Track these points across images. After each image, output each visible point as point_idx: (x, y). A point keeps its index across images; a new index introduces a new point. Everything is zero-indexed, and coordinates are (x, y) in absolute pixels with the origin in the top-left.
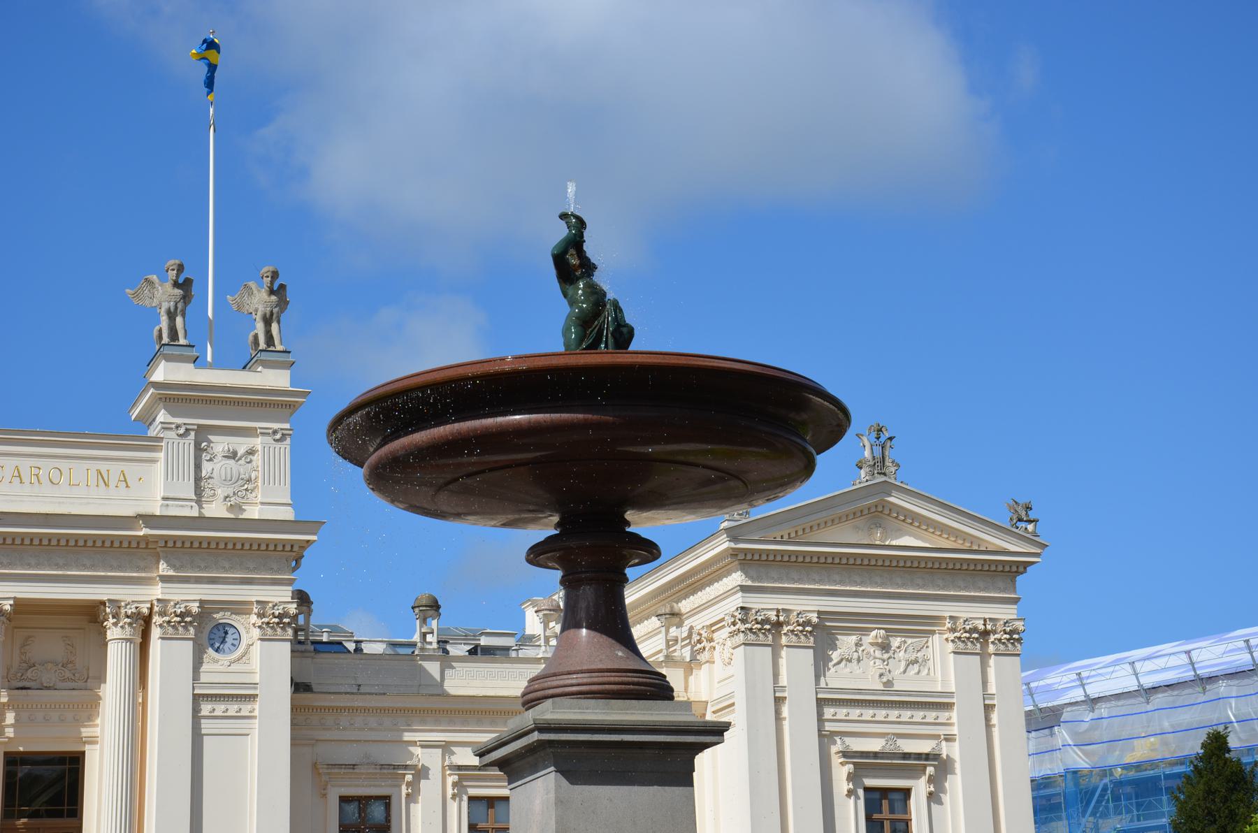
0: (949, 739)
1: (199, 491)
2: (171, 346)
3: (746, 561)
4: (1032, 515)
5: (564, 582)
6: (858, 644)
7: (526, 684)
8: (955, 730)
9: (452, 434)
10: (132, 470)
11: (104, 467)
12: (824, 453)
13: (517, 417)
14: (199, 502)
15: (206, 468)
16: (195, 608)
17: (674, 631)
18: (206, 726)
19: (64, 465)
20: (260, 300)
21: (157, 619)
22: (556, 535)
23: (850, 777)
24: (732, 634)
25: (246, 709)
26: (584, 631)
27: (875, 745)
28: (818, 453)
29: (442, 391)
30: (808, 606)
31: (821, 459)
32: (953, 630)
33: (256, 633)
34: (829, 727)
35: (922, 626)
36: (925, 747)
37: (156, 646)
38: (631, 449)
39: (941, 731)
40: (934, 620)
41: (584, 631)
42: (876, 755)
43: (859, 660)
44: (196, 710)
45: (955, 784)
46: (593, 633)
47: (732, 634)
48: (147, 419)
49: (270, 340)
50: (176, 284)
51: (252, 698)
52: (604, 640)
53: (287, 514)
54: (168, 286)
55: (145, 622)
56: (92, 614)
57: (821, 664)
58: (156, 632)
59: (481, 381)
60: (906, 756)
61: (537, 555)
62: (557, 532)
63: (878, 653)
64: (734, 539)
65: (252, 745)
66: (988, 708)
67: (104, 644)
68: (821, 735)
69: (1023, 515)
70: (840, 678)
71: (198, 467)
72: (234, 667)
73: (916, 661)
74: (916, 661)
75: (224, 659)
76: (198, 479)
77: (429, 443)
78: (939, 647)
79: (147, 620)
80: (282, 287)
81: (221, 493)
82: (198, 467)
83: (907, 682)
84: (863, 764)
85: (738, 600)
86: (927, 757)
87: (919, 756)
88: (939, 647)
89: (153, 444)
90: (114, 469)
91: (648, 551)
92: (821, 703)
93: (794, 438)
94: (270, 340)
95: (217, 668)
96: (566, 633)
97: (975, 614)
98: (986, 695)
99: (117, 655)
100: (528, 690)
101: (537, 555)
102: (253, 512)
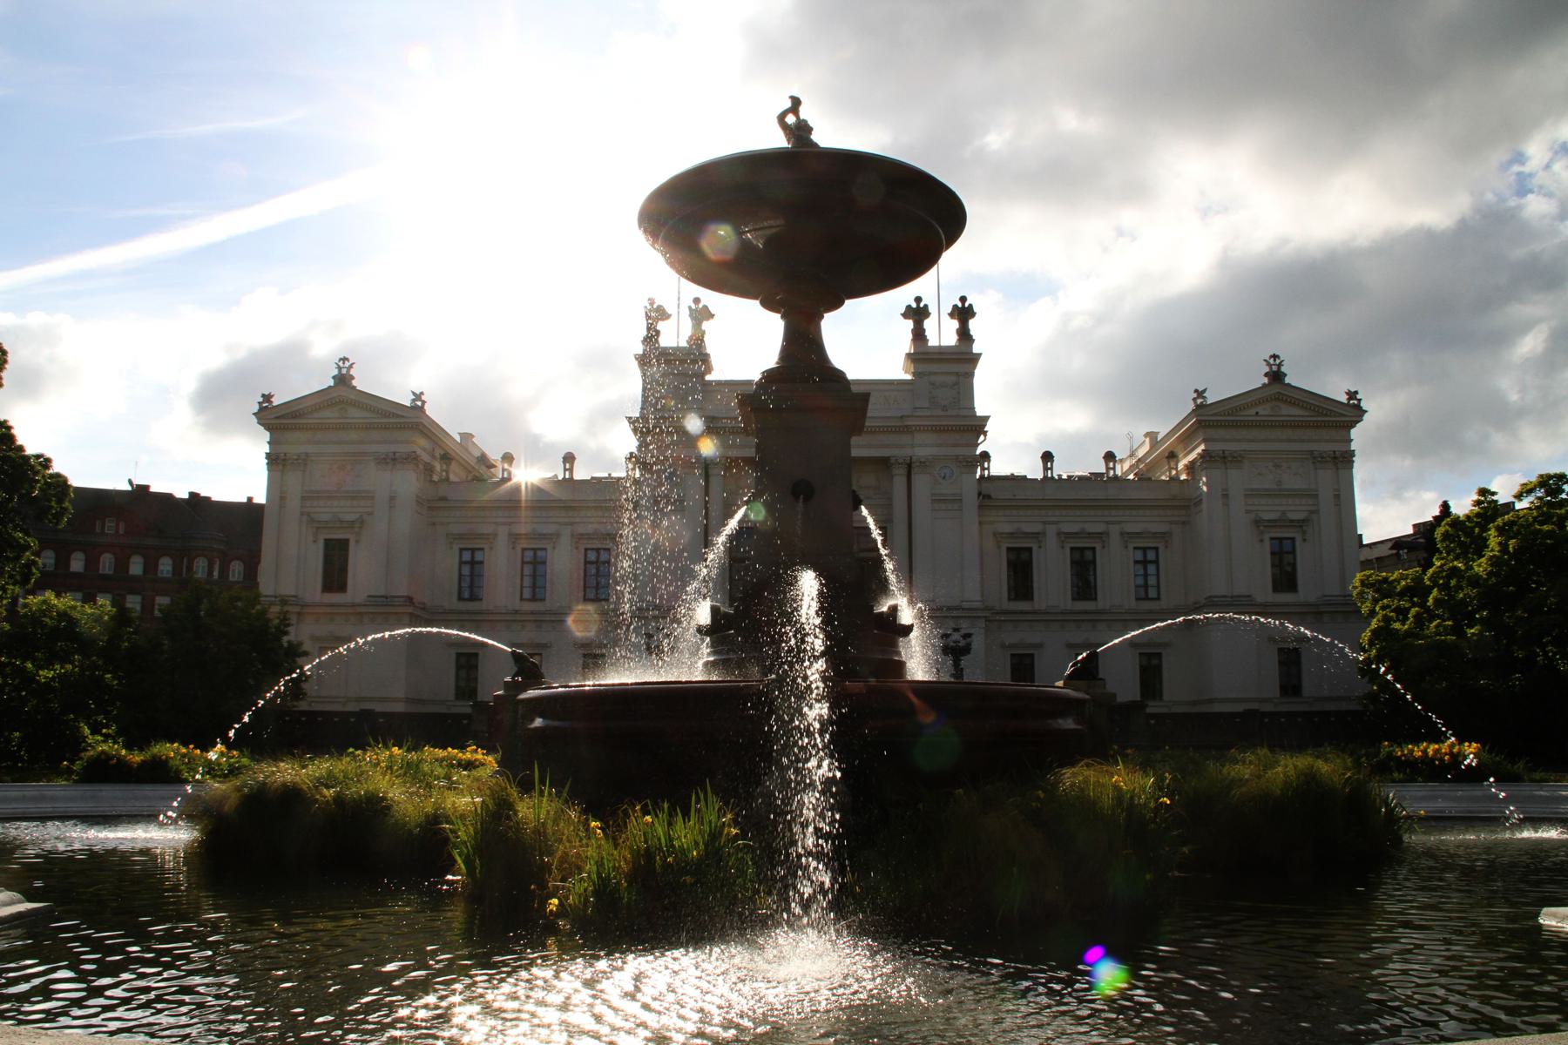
55: (909, 467)
60: (1292, 521)
64: (1197, 416)
92: (934, 501)
99: (899, 483)
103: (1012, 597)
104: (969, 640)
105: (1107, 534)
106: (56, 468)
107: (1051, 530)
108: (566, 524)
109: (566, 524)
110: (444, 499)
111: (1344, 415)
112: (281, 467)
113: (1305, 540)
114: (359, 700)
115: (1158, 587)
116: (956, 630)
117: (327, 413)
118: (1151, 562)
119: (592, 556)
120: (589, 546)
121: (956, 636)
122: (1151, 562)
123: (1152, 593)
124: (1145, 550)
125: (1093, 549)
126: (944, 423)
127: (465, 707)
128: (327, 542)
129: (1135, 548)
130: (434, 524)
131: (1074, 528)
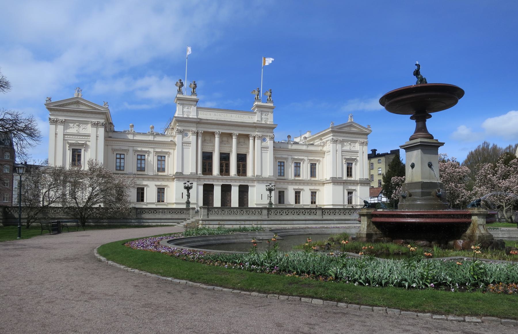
0: (358, 157)
1: (261, 119)
2: (258, 100)
3: (333, 131)
4: (370, 127)
6: (73, 125)
8: (359, 155)
10: (253, 116)
11: (249, 116)
14: (183, 115)
15: (262, 117)
16: (64, 120)
17: (321, 141)
18: (184, 147)
19: (244, 115)
20: (269, 93)
21: (256, 137)
23: (345, 161)
24: (330, 142)
25: (267, 150)
27: (349, 157)
30: (341, 139)
32: (91, 123)
33: (269, 139)
34: (343, 155)
35: (355, 142)
36: (355, 158)
37: (256, 140)
39: (357, 156)
40: (89, 121)
42: (349, 158)
43: (74, 128)
44: (182, 145)
45: (358, 164)
47: (330, 142)
48: (254, 110)
49: (258, 98)
50: (258, 91)
51: (190, 143)
53: (272, 123)
54: (257, 91)
55: (255, 137)
56: (213, 134)
57: (342, 147)
58: (256, 139)
60: (352, 159)
63: (77, 127)
64: (332, 129)
65: (268, 154)
66: (363, 153)
67: (249, 140)
68: (64, 140)
69: (369, 126)
70: (69, 131)
71: (261, 116)
72: (188, 139)
73: (84, 128)
74: (84, 128)
75: (265, 143)
76: (183, 111)
78: (357, 145)
79: (255, 137)
80: (196, 84)
81: (264, 120)
82: (261, 116)
83: (353, 149)
84: (347, 159)
85: (332, 137)
86: (355, 159)
87: (354, 159)
88: (357, 145)
89: (256, 113)
90: (250, 116)
92: (342, 151)
94: (258, 98)
95: (264, 144)
97: (362, 140)
98: (363, 151)
99: (251, 141)
100: (414, 135)
102: (191, 117)
103: (138, 170)
104: (192, 185)
105: (288, 158)
106: (473, 150)
107: (131, 149)
108: (131, 147)
109: (131, 147)
110: (110, 137)
111: (101, 110)
112: (63, 124)
113: (127, 154)
114: (320, 205)
115: (284, 173)
116: (188, 182)
117: (346, 129)
118: (282, 166)
119: (139, 157)
120: (117, 153)
121: (188, 183)
122: (282, 166)
123: (282, 174)
124: (281, 162)
125: (284, 162)
126: (178, 119)
127: (314, 206)
128: (73, 149)
129: (278, 162)
130: (107, 145)
131: (279, 156)
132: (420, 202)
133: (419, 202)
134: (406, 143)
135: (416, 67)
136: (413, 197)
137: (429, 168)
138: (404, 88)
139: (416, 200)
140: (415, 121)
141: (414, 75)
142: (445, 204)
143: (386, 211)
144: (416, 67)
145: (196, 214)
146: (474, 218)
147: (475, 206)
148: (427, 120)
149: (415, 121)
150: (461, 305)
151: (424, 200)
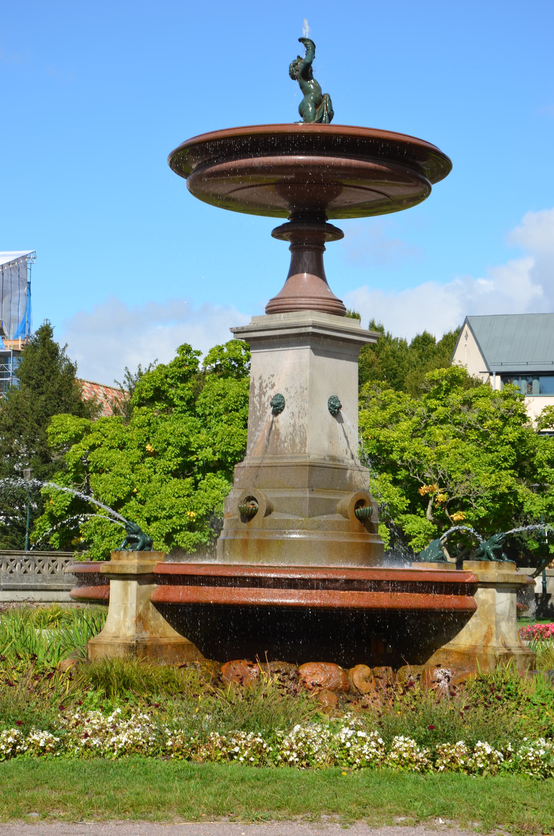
5: (292, 248)
7: (268, 302)
9: (260, 163)
12: (346, 362)
13: (301, 158)
22: (288, 223)
26: (305, 274)
28: (434, 182)
29: (247, 144)
31: (434, 187)
38: (377, 166)
41: (305, 274)
46: (310, 275)
52: (315, 278)
59: (372, 141)
61: (278, 233)
62: (289, 221)
77: (282, 164)
91: (337, 234)
93: (420, 176)
96: (292, 278)
100: (270, 305)
101: (278, 233)
132: (300, 534)
133: (296, 533)
134: (253, 318)
135: (301, 51)
136: (275, 516)
137: (330, 416)
138: (248, 131)
139: (290, 526)
140: (288, 244)
141: (293, 77)
142: (449, 528)
143: (172, 562)
144: (301, 51)
145: (364, 710)
146: (481, 594)
147: (489, 558)
148: (327, 245)
149: (288, 244)
150: (113, 739)
151: (318, 528)
